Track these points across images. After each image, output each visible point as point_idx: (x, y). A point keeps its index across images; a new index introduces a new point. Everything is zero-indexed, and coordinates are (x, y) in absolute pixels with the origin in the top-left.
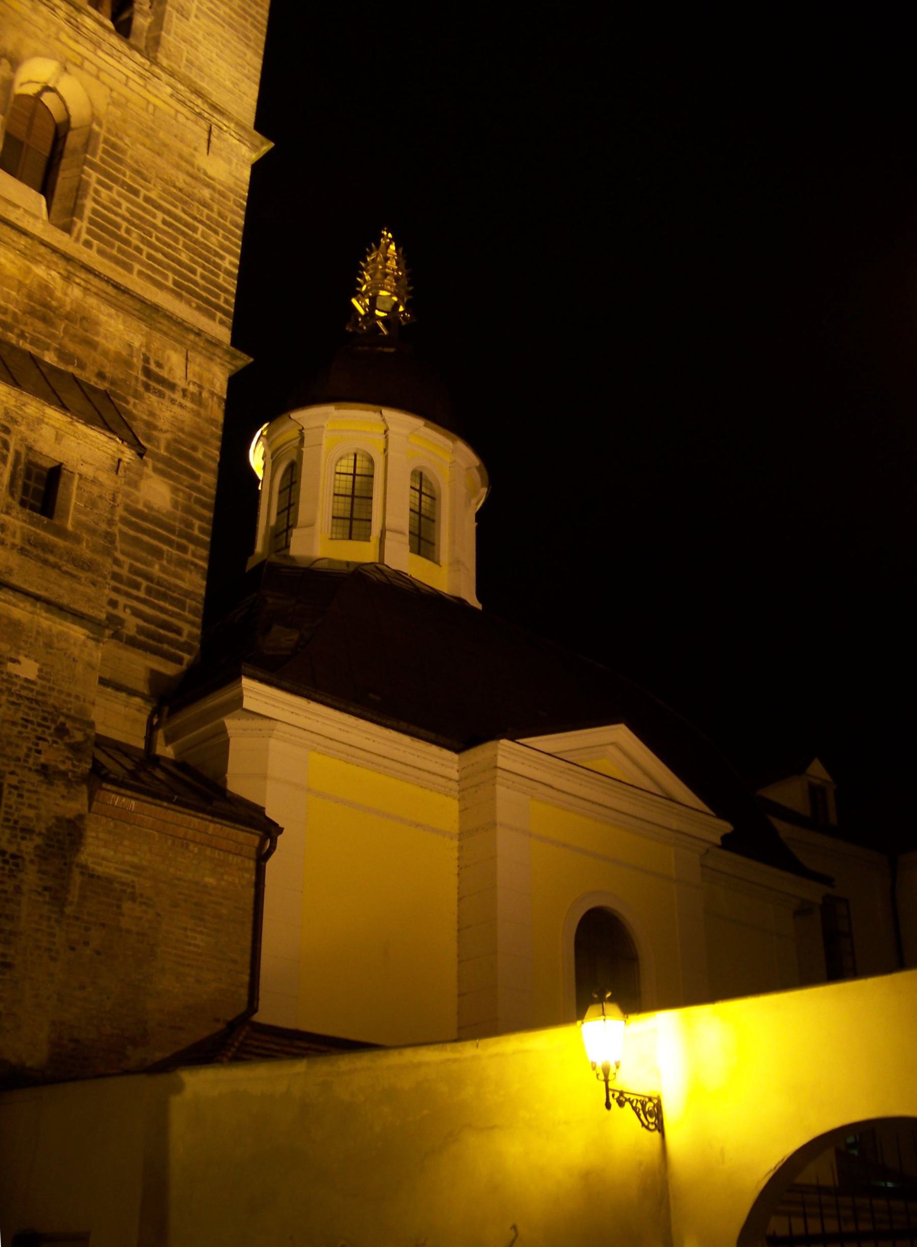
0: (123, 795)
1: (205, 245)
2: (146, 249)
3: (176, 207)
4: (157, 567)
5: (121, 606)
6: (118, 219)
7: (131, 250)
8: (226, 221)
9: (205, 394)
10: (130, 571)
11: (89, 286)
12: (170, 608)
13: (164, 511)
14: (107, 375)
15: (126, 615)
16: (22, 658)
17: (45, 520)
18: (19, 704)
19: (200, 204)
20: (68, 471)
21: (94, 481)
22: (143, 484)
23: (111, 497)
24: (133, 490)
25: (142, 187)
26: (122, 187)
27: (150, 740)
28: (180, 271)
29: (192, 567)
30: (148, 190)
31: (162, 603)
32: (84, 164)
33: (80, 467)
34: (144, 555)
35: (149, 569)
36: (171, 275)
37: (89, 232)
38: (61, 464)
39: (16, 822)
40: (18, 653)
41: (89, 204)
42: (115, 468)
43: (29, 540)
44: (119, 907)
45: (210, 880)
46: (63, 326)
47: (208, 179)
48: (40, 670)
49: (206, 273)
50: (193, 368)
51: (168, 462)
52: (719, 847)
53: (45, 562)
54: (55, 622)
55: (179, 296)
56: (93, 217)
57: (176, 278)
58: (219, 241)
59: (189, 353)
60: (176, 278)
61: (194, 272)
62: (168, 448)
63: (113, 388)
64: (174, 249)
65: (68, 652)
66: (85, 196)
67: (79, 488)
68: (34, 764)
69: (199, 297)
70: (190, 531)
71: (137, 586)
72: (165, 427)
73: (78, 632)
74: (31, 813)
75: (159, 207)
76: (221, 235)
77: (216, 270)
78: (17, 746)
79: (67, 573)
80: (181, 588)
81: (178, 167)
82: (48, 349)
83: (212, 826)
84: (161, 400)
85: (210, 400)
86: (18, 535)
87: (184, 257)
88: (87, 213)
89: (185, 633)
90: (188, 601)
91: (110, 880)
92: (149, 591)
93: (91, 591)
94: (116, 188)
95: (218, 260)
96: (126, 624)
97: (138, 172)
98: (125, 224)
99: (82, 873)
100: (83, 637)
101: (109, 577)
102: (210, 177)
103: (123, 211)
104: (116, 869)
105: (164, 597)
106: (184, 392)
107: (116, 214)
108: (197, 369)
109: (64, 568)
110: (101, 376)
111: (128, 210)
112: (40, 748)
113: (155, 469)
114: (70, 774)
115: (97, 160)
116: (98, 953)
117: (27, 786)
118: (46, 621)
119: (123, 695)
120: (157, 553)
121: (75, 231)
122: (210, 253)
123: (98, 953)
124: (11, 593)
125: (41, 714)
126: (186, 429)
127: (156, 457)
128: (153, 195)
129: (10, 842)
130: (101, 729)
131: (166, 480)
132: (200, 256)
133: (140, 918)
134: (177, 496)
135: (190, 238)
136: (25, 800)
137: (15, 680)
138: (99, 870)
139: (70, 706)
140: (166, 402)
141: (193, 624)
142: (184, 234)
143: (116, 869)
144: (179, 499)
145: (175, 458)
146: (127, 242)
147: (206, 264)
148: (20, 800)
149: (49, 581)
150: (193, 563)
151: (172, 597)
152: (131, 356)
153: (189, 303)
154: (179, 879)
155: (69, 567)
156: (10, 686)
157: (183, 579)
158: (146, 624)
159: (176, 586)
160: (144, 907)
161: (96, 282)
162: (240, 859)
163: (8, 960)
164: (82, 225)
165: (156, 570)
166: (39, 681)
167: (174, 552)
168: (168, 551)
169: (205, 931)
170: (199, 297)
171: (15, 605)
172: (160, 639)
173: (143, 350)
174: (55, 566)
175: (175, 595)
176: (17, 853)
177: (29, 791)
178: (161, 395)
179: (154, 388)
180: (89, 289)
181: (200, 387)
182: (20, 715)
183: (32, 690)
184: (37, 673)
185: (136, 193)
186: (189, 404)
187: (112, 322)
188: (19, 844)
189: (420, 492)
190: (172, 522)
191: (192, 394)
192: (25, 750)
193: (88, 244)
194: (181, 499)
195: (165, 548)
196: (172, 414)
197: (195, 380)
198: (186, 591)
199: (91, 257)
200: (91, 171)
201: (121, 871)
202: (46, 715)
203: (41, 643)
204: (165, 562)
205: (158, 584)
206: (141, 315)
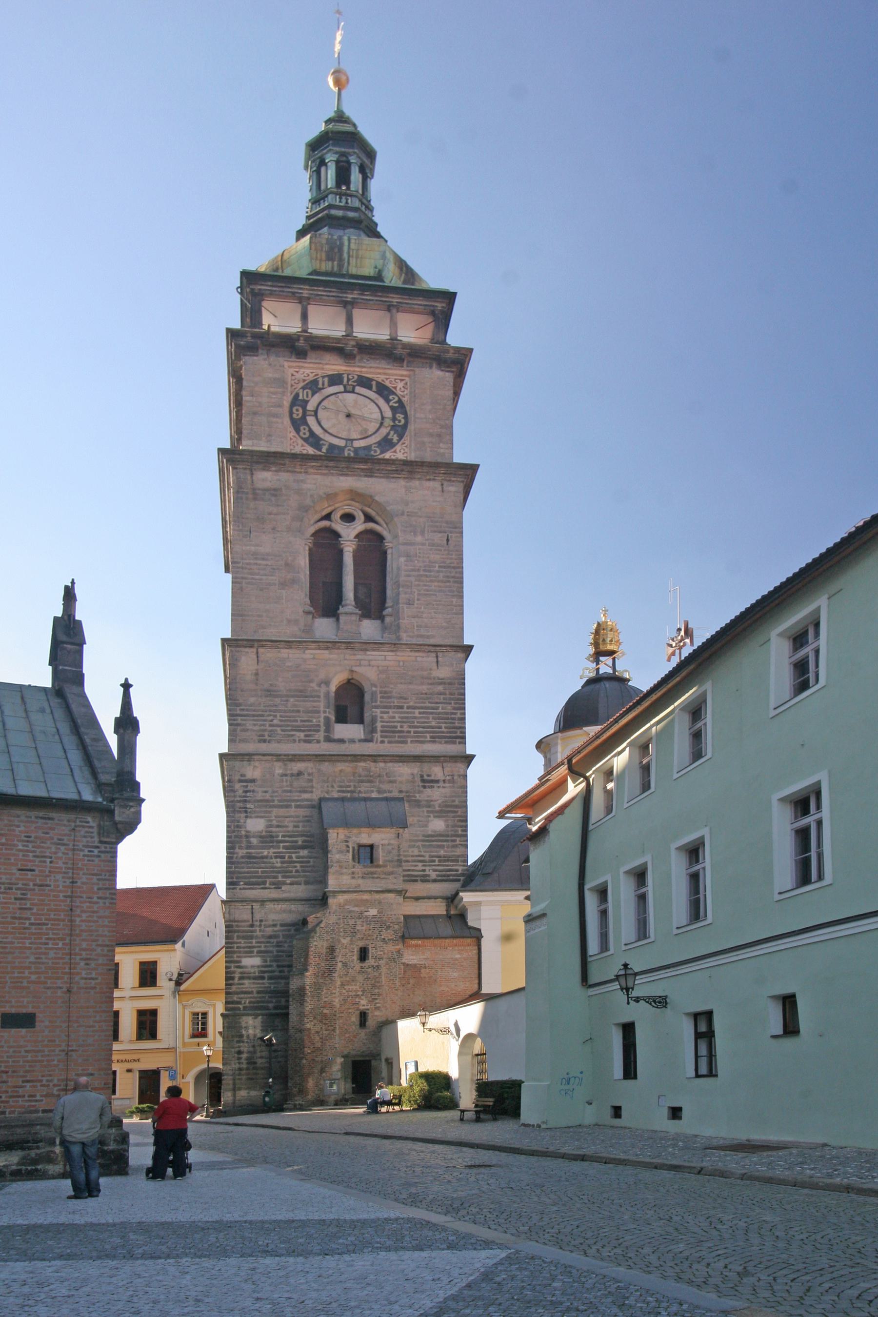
3: (425, 703)
45: (458, 956)
51: (441, 811)
71: (434, 861)
74: (382, 953)
88: (379, 729)
105: (448, 861)
110: (401, 792)
118: (377, 896)
120: (442, 847)
128: (411, 704)
140: (435, 789)
153: (440, 743)
161: (387, 758)
172: (448, 876)
174: (377, 878)
191: (449, 780)
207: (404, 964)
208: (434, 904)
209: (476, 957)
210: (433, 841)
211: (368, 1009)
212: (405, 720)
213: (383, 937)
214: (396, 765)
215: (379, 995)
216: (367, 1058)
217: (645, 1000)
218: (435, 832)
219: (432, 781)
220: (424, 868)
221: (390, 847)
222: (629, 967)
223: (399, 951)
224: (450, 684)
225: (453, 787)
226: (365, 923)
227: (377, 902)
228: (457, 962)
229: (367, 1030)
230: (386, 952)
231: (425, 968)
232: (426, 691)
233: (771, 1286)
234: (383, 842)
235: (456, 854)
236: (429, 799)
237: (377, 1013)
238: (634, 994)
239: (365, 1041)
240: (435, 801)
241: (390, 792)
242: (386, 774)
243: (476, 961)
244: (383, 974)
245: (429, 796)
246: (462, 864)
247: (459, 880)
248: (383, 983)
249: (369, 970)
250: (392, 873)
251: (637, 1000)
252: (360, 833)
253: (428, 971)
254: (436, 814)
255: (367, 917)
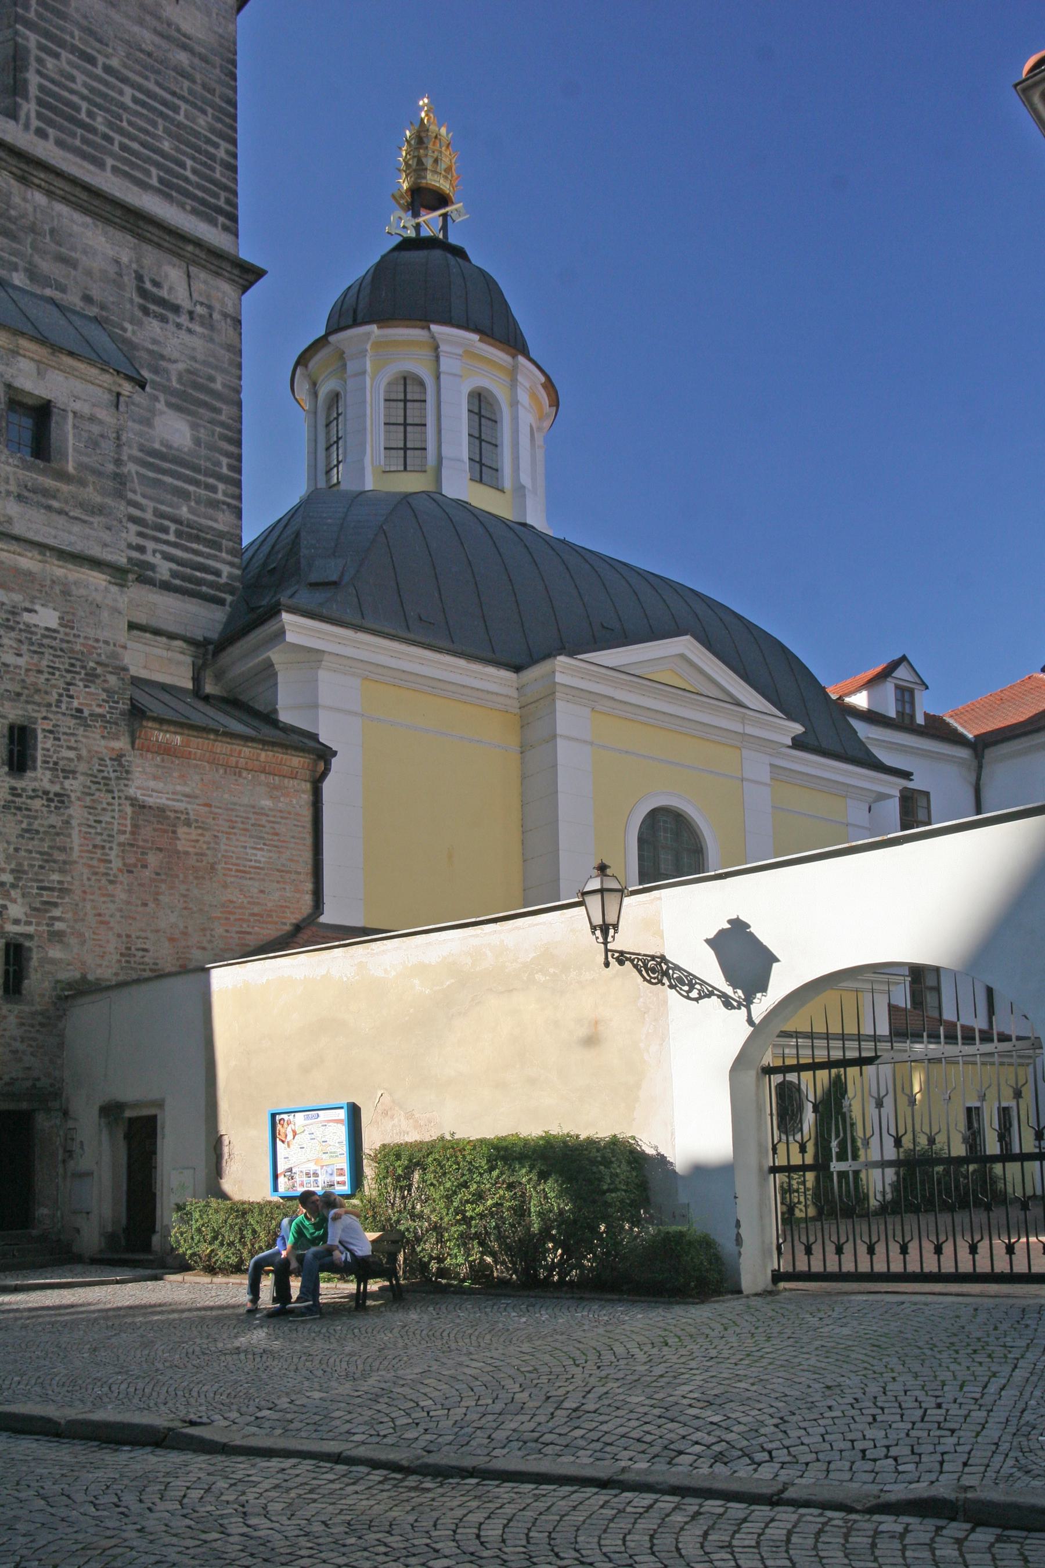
0: (167, 731)
1: (191, 128)
2: (117, 137)
3: (147, 78)
4: (185, 509)
5: (149, 551)
6: (75, 99)
7: (98, 140)
8: (214, 95)
9: (216, 316)
10: (155, 515)
11: (52, 188)
12: (207, 550)
13: (186, 449)
14: (95, 298)
15: (157, 560)
16: (37, 607)
17: (41, 464)
18: (43, 653)
19: (178, 73)
20: (59, 408)
21: (92, 419)
22: (157, 421)
23: (114, 435)
24: (146, 429)
25: (99, 52)
26: (72, 53)
27: (197, 679)
28: (163, 165)
29: (225, 507)
30: (107, 56)
31: (195, 546)
32: (16, 22)
33: (73, 404)
34: (169, 497)
35: (177, 512)
36: (154, 171)
37: (40, 116)
38: (50, 401)
39: (56, 763)
40: (32, 602)
41: (33, 80)
42: (115, 402)
43: (26, 487)
44: (174, 832)
45: (267, 803)
46: (29, 240)
47: (183, 39)
48: (61, 618)
49: (198, 167)
50: (198, 286)
51: (182, 395)
52: (789, 747)
53: (49, 508)
54: (70, 570)
55: (168, 197)
56: (41, 95)
57: (162, 174)
58: (207, 122)
59: (191, 268)
60: (162, 174)
61: (183, 165)
62: (180, 379)
63: (104, 313)
64: (154, 136)
65: (90, 599)
66: (25, 68)
67: (75, 426)
68: (67, 709)
69: (194, 198)
70: (217, 469)
71: (165, 530)
72: (175, 355)
73: (98, 579)
74: (72, 754)
75: (125, 80)
76: (210, 116)
77: (209, 162)
78: (46, 693)
79: (76, 518)
80: (214, 529)
81: (141, 23)
82: (16, 270)
83: (263, 754)
84: (164, 325)
85: (223, 323)
86: (12, 481)
87: (166, 146)
88: (33, 91)
89: (225, 574)
90: (224, 542)
91: (161, 810)
92: (179, 534)
93: (106, 536)
94: (64, 54)
95: (212, 150)
96: (158, 569)
97: (91, 32)
98: (84, 105)
99: (132, 805)
100: (104, 583)
101: (124, 520)
102: (185, 35)
103: (78, 87)
104: (168, 799)
105: (197, 539)
106: (191, 313)
107: (72, 92)
108: (202, 286)
109: (72, 514)
110: (88, 299)
111: (85, 85)
112: (71, 693)
113: (169, 405)
114: (108, 716)
115: (32, 15)
116: (158, 874)
117: (61, 730)
118: (59, 570)
119: (164, 640)
120: (185, 495)
121: (22, 114)
122: (199, 139)
123: (158, 874)
124: (14, 542)
125: (67, 661)
126: (200, 357)
127: (167, 390)
128: (115, 63)
129: (52, 782)
130: (134, 671)
131: (183, 416)
132: (188, 144)
133: (197, 841)
134: (198, 432)
135: (172, 121)
136: (62, 743)
137: (33, 629)
138: (150, 801)
139: (99, 651)
140: (171, 327)
141: (232, 564)
142: (161, 114)
143: (168, 799)
144: (201, 436)
145: (190, 391)
146: (93, 130)
147: (197, 155)
148: (57, 743)
149: (56, 528)
150: (224, 503)
151: (205, 539)
152: (120, 275)
153: (182, 206)
154: (235, 804)
155: (76, 513)
156: (29, 636)
157: (216, 521)
158: (180, 568)
159: (211, 528)
160: (200, 831)
161: (59, 183)
162: (296, 782)
163: (66, 886)
164: (29, 108)
165: (184, 512)
166: (62, 629)
167: (203, 492)
168: (195, 492)
169: (266, 847)
170: (194, 198)
171: (19, 554)
172: (199, 582)
173: (134, 266)
174: (60, 512)
175: (209, 537)
176: (62, 792)
177: (65, 734)
178: (163, 319)
179: (154, 312)
180: (53, 193)
181: (210, 307)
182: (45, 663)
183: (55, 639)
184: (58, 621)
185: (92, 60)
186: (198, 329)
187: (89, 234)
188: (62, 783)
189: (480, 416)
190: (195, 460)
191: (201, 316)
192: (56, 696)
193: (41, 133)
194: (202, 434)
195: (191, 488)
196: (179, 341)
197: (201, 300)
198: (221, 531)
199: (46, 150)
200: (28, 32)
201: (173, 800)
202: (73, 661)
203: (58, 592)
204: (193, 504)
205: (189, 526)
206: (124, 223)
207: (133, 801)
208: (165, 653)
209: (307, 814)
210: (164, 472)
211: (29, 937)
212: (99, 100)
213: (76, 704)
214: (78, 217)
215: (63, 891)
216: (24, 1105)
217: (632, 961)
218: (169, 447)
219: (162, 302)
220: (141, 541)
221: (96, 429)
222: (609, 871)
223: (118, 758)
224: (204, 59)
225: (211, 340)
226: (25, 647)
227: (57, 589)
228: (263, 820)
229: (26, 1008)
230: (84, 753)
231: (188, 823)
232: (150, 48)
233: (482, 1543)
234: (77, 406)
235: (215, 525)
236: (155, 348)
237: (55, 952)
238: (620, 942)
239: (17, 1045)
240: (169, 360)
241: (63, 289)
242: (52, 231)
243: (309, 826)
244: (74, 823)
245: (155, 341)
246: (229, 558)
247: (221, 602)
248: (75, 855)
249: (37, 804)
250: (99, 510)
251: (622, 958)
252: (15, 353)
253: (194, 834)
254: (173, 400)
255: (29, 628)
